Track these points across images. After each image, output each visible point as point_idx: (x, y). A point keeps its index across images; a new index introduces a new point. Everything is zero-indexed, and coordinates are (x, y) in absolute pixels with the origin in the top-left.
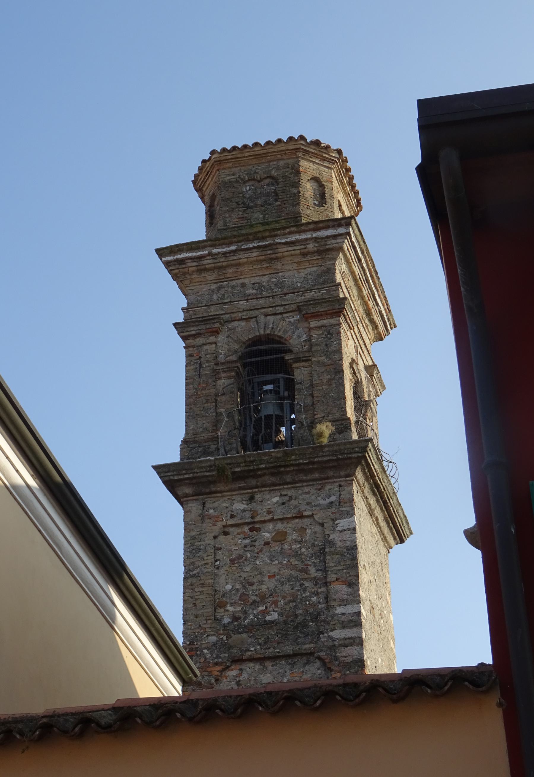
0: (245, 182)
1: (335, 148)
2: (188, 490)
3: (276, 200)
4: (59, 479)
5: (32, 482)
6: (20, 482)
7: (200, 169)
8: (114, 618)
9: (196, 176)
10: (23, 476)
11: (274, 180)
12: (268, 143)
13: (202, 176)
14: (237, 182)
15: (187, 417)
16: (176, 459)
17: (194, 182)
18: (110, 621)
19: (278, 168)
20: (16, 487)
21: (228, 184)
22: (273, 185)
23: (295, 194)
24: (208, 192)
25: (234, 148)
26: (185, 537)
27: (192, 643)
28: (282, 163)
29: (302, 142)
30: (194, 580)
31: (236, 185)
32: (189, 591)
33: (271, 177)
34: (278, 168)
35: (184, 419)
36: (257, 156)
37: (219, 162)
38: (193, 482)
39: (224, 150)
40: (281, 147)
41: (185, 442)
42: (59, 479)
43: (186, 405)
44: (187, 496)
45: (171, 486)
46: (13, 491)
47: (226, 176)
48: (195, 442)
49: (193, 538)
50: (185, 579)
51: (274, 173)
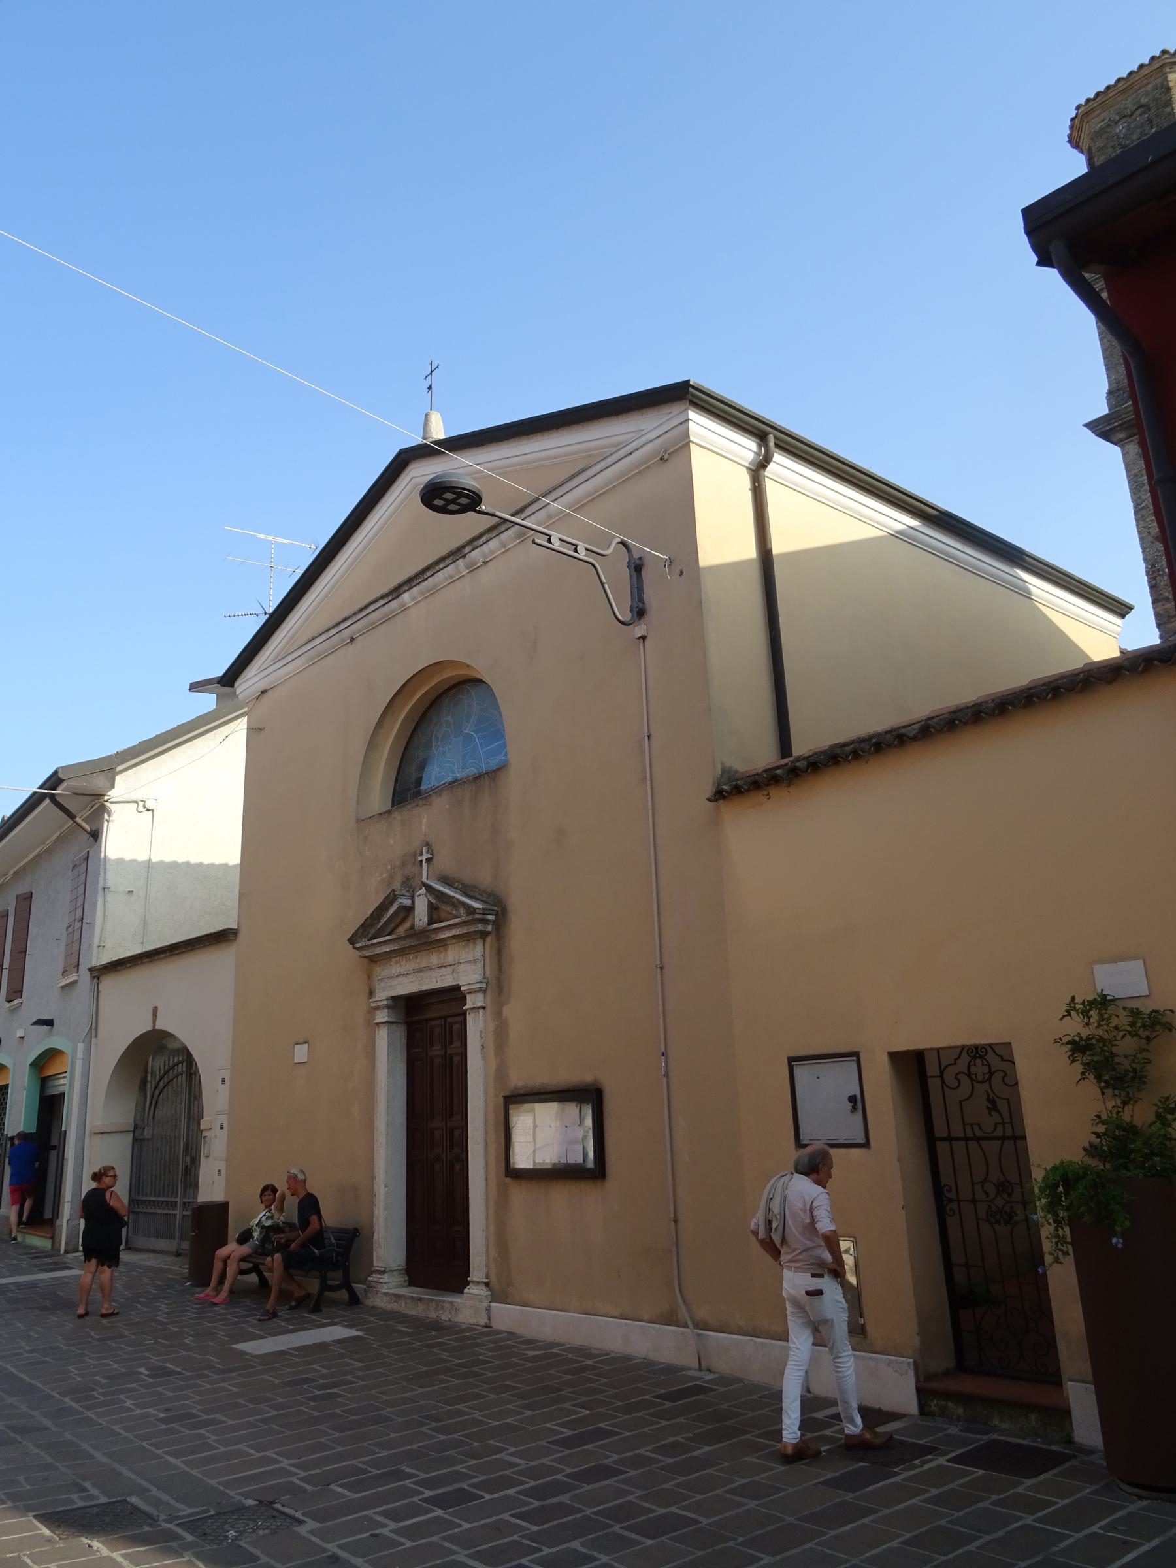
0: (1116, 123)
1: (416, 902)
2: (1121, 435)
3: (1152, 128)
4: (935, 512)
5: (914, 523)
6: (902, 527)
7: (1071, 128)
8: (1029, 592)
9: (1070, 136)
10: (904, 521)
11: (1145, 107)
12: (1131, 73)
13: (1076, 132)
14: (1109, 126)
15: (1107, 370)
16: (1105, 411)
17: (1070, 142)
18: (1026, 594)
19: (1147, 94)
20: (899, 532)
21: (1098, 134)
22: (1144, 113)
23: (1169, 114)
24: (1085, 145)
25: (1098, 94)
26: (1128, 476)
27: (1153, 566)
28: (1150, 86)
29: (1166, 56)
30: (1144, 512)
31: (1108, 130)
32: (1142, 523)
33: (1142, 106)
34: (1147, 94)
35: (1105, 372)
36: (1123, 91)
37: (1086, 114)
38: (1124, 426)
39: (1088, 100)
40: (1145, 71)
41: (1110, 393)
42: (935, 512)
43: (1104, 358)
44: (1121, 440)
45: (1105, 435)
46: (899, 536)
47: (1096, 124)
48: (1118, 390)
49: (1136, 475)
50: (1135, 513)
51: (1144, 101)
